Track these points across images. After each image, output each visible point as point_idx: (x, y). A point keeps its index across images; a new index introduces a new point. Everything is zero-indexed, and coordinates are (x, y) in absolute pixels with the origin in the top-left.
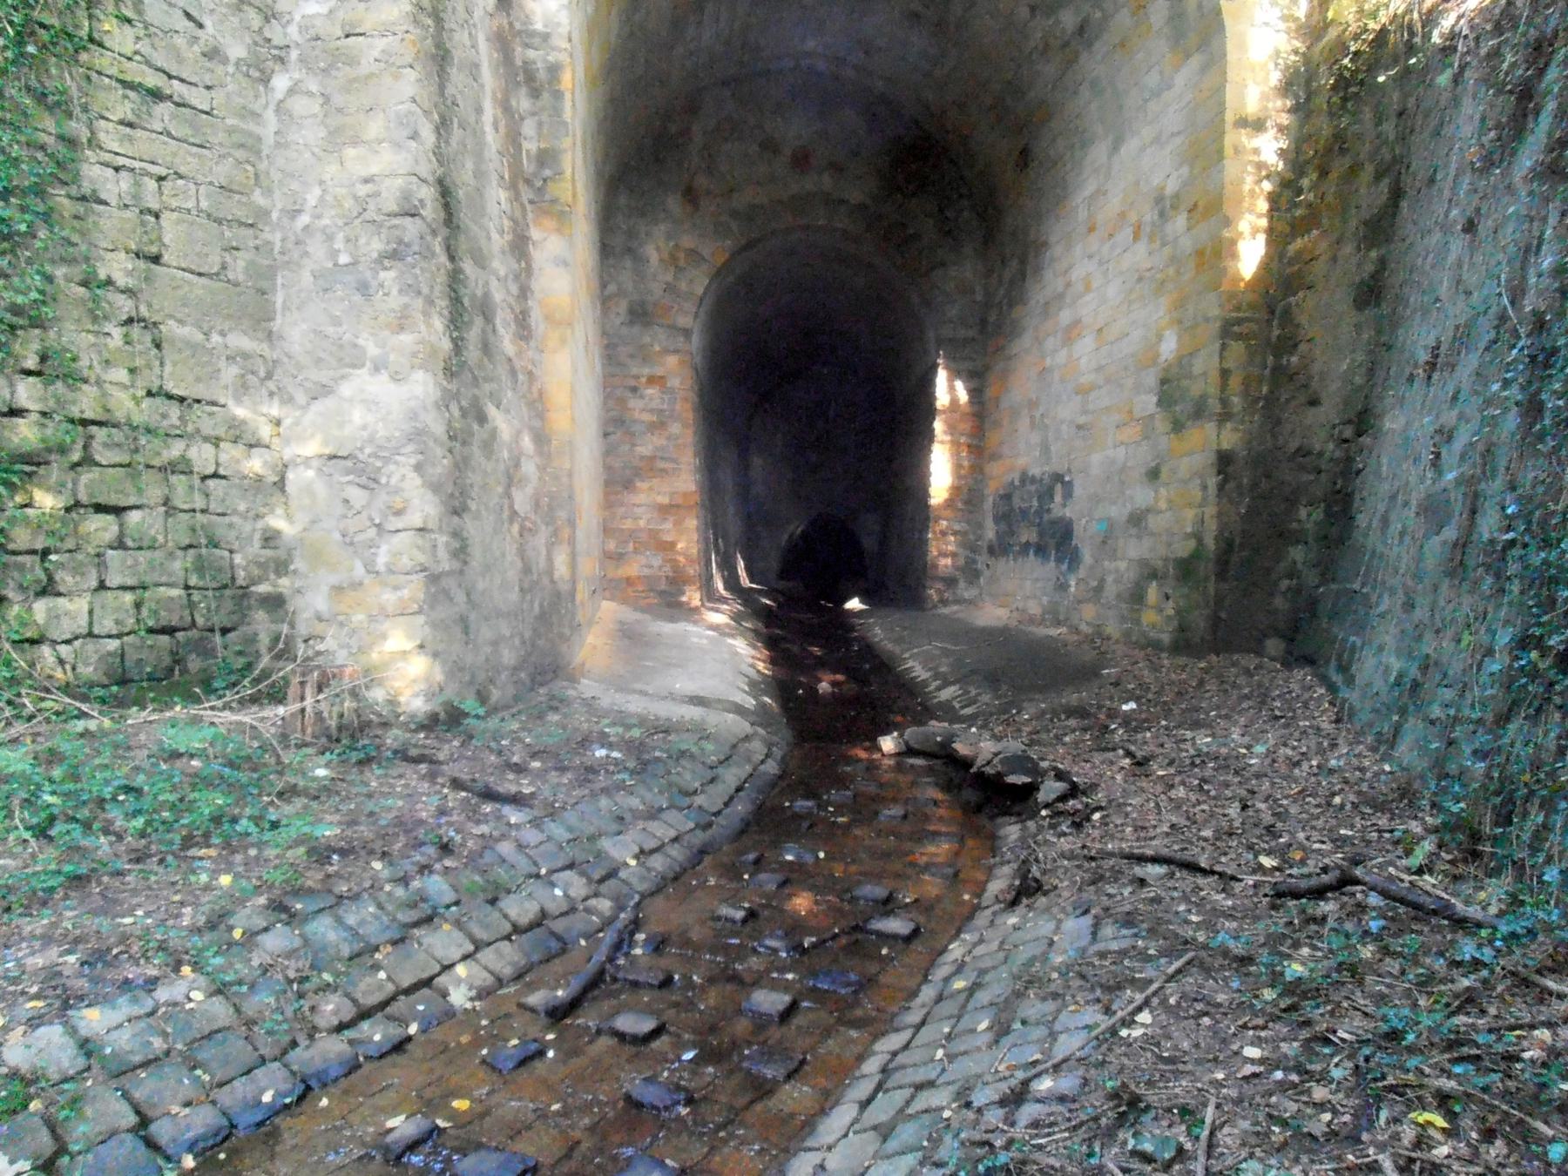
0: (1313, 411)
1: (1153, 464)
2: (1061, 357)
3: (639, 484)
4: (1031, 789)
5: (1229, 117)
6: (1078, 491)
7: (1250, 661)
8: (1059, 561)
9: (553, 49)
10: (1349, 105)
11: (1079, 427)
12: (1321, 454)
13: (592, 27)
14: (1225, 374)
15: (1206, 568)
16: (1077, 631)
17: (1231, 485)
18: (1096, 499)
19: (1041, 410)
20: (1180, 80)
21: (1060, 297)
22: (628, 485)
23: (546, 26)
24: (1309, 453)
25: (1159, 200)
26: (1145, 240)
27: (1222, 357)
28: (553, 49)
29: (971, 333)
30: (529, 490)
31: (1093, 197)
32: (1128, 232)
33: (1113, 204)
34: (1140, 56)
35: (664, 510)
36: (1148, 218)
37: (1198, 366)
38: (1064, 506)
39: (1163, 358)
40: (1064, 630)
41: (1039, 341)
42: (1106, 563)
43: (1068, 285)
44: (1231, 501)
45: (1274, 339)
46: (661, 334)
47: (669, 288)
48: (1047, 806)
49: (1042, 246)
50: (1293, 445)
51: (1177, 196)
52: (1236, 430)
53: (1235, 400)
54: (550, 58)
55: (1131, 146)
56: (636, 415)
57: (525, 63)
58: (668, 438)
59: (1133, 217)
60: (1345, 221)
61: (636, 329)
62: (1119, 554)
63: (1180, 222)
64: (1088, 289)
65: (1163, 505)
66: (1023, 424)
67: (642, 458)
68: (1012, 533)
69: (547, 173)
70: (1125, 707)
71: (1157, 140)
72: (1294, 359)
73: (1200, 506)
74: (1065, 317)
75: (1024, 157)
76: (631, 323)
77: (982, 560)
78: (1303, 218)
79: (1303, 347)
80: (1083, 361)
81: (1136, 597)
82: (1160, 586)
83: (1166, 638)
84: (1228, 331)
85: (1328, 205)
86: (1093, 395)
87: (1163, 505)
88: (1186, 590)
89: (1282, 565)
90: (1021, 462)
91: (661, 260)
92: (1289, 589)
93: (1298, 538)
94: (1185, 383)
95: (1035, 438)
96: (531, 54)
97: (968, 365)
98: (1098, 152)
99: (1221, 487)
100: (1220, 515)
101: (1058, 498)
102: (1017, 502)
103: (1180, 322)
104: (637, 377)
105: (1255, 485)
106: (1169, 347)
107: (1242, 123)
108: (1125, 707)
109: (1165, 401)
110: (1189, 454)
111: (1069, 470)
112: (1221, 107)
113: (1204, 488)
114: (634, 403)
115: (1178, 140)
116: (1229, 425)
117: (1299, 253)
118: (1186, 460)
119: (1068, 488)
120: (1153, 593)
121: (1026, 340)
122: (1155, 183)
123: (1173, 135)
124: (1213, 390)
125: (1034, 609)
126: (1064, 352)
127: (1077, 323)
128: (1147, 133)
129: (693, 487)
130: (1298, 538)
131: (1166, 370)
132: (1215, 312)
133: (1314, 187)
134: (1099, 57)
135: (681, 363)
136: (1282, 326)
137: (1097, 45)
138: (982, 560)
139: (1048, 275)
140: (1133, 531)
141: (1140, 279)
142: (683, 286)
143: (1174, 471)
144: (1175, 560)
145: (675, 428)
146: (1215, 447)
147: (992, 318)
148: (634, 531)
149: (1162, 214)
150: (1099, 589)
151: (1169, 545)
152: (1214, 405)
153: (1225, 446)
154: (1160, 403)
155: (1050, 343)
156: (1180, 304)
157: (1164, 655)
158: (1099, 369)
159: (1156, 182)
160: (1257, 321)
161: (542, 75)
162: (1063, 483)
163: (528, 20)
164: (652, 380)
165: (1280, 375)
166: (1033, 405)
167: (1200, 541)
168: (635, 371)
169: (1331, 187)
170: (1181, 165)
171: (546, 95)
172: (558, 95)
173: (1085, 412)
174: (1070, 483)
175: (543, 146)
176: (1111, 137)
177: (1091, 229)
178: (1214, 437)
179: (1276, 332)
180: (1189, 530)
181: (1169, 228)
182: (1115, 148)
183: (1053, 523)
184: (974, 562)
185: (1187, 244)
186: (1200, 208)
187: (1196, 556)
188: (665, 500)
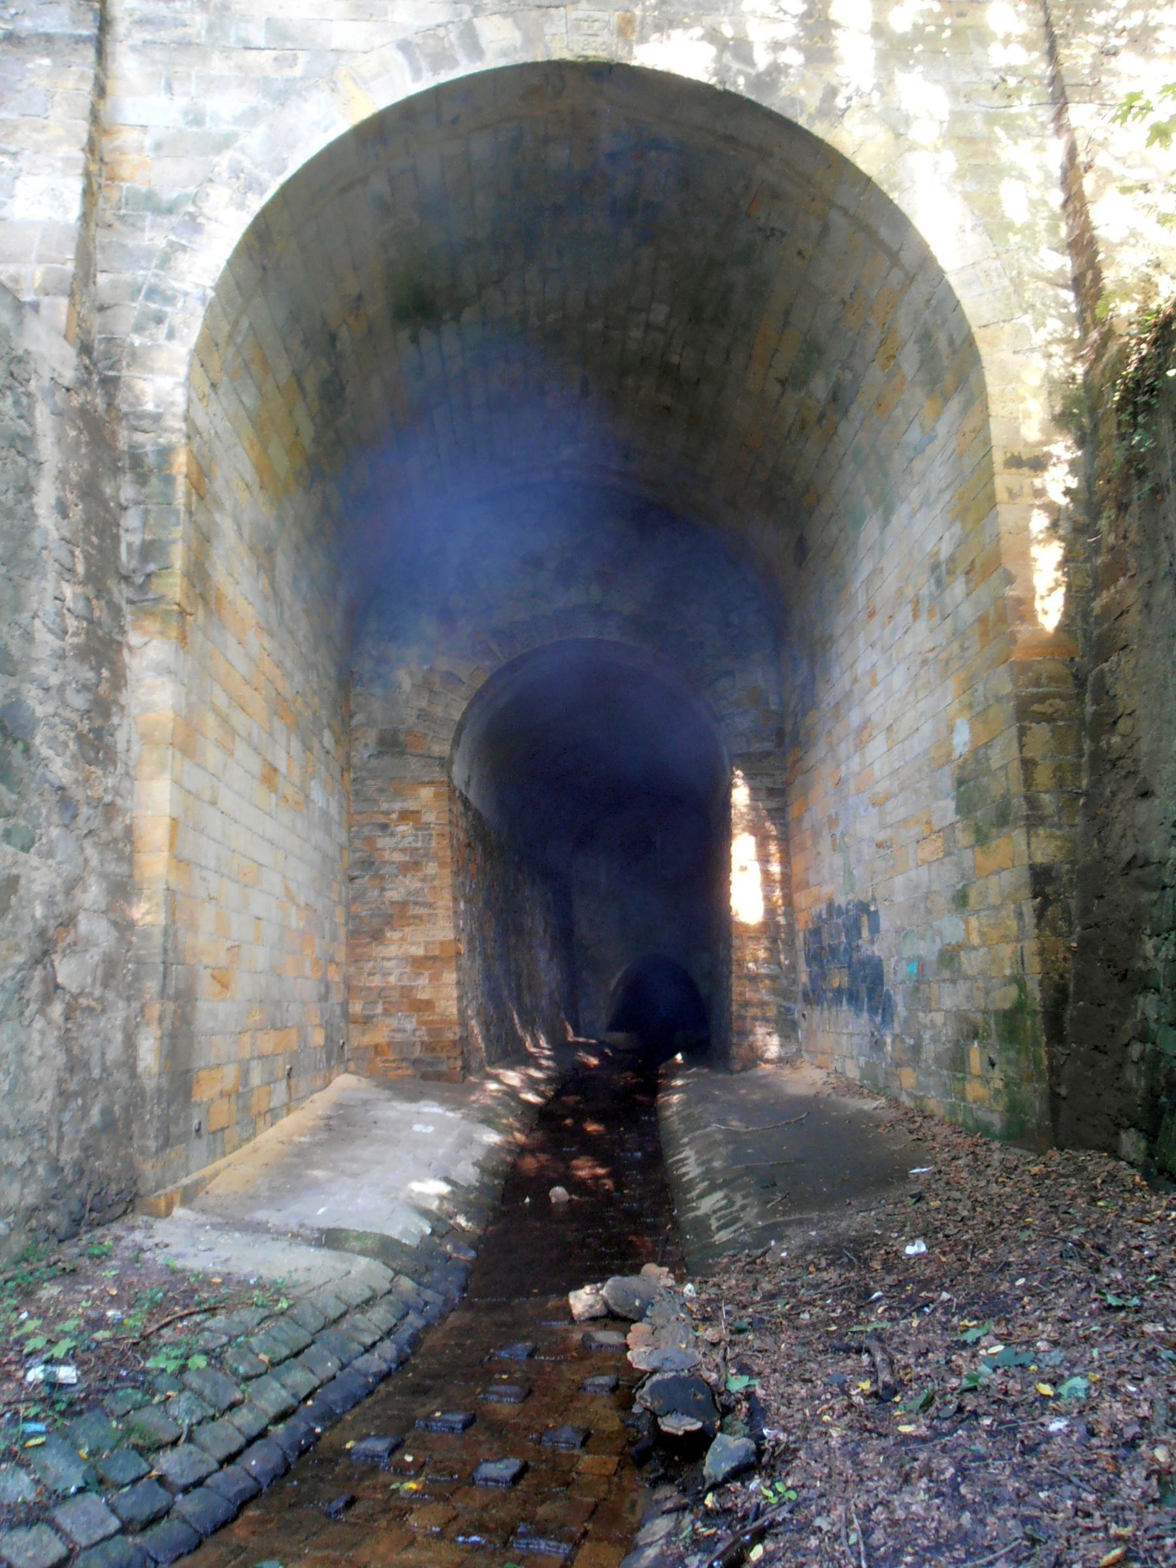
0: (1143, 806)
1: (959, 887)
2: (855, 764)
3: (388, 935)
4: (699, 1443)
5: (998, 457)
6: (884, 924)
7: (1098, 1165)
8: (873, 1011)
9: (165, 430)
10: (1140, 419)
11: (879, 845)
12: (1162, 863)
13: (260, 425)
14: (1028, 765)
15: (1034, 1025)
16: (895, 1102)
17: (1050, 911)
18: (902, 933)
19: (841, 827)
20: (942, 429)
21: (848, 695)
22: (377, 936)
23: (158, 406)
24: (1147, 863)
25: (935, 567)
26: (924, 616)
27: (1022, 746)
28: (165, 430)
29: (768, 746)
30: (94, 956)
31: (869, 579)
32: (907, 610)
33: (890, 583)
34: (898, 412)
35: (418, 963)
36: (925, 591)
37: (996, 759)
38: (872, 942)
39: (956, 755)
40: (882, 1101)
41: (832, 748)
42: (921, 1015)
43: (855, 680)
44: (1055, 931)
45: (1088, 718)
46: (414, 765)
47: (423, 715)
48: (714, 1487)
49: (827, 641)
50: (1126, 854)
51: (952, 559)
52: (1051, 837)
53: (1046, 798)
54: (162, 440)
55: (902, 511)
56: (387, 855)
57: (131, 447)
58: (423, 880)
59: (910, 592)
60: (1156, 559)
61: (387, 760)
62: (933, 1005)
63: (959, 588)
64: (874, 683)
65: (975, 940)
66: (825, 845)
67: (392, 903)
68: (824, 976)
69: (152, 567)
70: (910, 1250)
71: (926, 503)
72: (1116, 740)
73: (1018, 940)
74: (855, 717)
75: (801, 549)
76: (381, 754)
77: (798, 1008)
78: (1106, 566)
79: (1124, 725)
80: (876, 766)
81: (957, 1062)
82: (983, 1047)
83: (996, 1121)
84: (1025, 713)
85: (1134, 546)
86: (889, 806)
87: (975, 940)
88: (1012, 1054)
89: (1128, 1025)
90: (826, 890)
91: (413, 685)
92: (1142, 1058)
93: (1144, 983)
94: (985, 780)
95: (837, 860)
96: (139, 437)
97: (768, 782)
98: (870, 530)
99: (1040, 914)
100: (1042, 952)
101: (865, 933)
102: (826, 940)
103: (970, 706)
104: (387, 813)
105: (1086, 911)
106: (962, 739)
107: (1015, 462)
108: (910, 1250)
109: (965, 807)
110: (998, 872)
111: (874, 899)
112: (987, 443)
113: (1020, 915)
114: (384, 842)
115: (947, 496)
116: (1041, 832)
117: (1106, 609)
118: (994, 879)
119: (874, 916)
120: (976, 1058)
121: (820, 750)
122: (929, 548)
123: (942, 491)
124: (1017, 787)
125: (853, 1072)
126: (857, 759)
127: (866, 723)
128: (915, 495)
129: (450, 935)
130: (1144, 983)
131: (962, 767)
132: (1007, 688)
133: (1114, 525)
134: (857, 423)
135: (437, 795)
136: (1096, 701)
137: (853, 410)
138: (798, 1008)
139: (836, 672)
140: (946, 974)
141: (925, 662)
142: (439, 711)
143: (983, 895)
144: (996, 1012)
145: (431, 868)
146: (1026, 861)
147: (789, 728)
148: (383, 989)
149: (939, 582)
150: (916, 1049)
151: (987, 992)
152: (1019, 806)
153: (1039, 858)
154: (958, 810)
155: (843, 749)
156: (969, 685)
157: (995, 1145)
158: (894, 772)
159: (929, 547)
160: (1061, 696)
161: (151, 460)
162: (869, 913)
163: (138, 401)
164: (404, 816)
165: (1102, 762)
166: (833, 822)
167: (1022, 987)
168: (385, 806)
169: (1131, 522)
170: (952, 523)
171: (154, 481)
172: (169, 480)
173: (883, 826)
174: (876, 912)
175: (148, 537)
176: (881, 509)
177: (872, 614)
178: (1024, 847)
179: (1090, 709)
180: (1008, 972)
181: (947, 598)
182: (886, 520)
183: (863, 964)
184: (788, 1010)
185: (968, 612)
186: (978, 565)
187: (1019, 1008)
188: (421, 952)
